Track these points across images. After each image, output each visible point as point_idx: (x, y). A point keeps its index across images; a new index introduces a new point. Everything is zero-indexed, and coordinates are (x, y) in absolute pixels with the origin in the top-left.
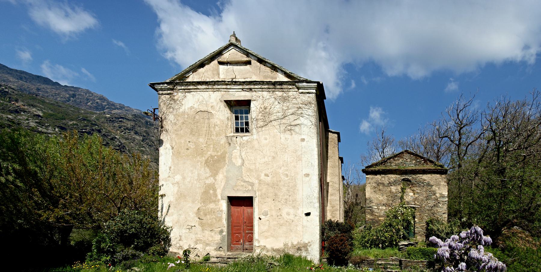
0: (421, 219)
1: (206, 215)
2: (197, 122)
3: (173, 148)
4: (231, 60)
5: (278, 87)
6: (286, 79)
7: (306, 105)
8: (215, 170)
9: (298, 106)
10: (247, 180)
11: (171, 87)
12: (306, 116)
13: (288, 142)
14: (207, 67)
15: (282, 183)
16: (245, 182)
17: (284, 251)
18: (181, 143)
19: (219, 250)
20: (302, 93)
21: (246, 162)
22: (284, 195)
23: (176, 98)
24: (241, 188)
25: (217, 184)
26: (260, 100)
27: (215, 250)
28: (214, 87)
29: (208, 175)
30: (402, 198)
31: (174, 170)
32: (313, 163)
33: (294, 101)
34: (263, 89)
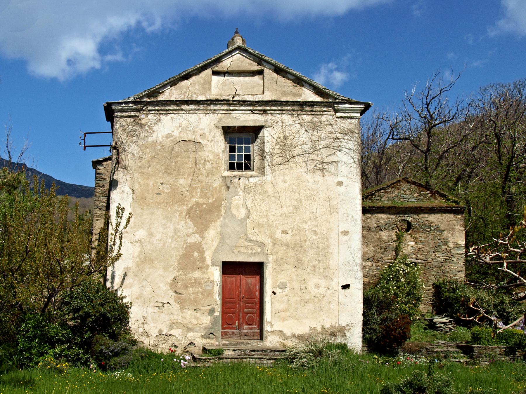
0: (427, 279)
1: (187, 287)
2: (177, 156)
3: (133, 192)
4: (234, 69)
5: (307, 109)
6: (318, 99)
7: (346, 134)
8: (202, 224)
9: (334, 136)
10: (254, 239)
11: (138, 107)
12: (345, 150)
13: (319, 186)
14: (194, 79)
15: (308, 243)
16: (250, 241)
17: (310, 336)
18: (148, 185)
19: (209, 338)
20: (341, 117)
21: (253, 214)
22: (311, 261)
23: (143, 122)
24: (245, 251)
25: (206, 244)
26: (277, 128)
27: (203, 337)
28: (209, 108)
29: (191, 231)
30: (397, 249)
31: (134, 222)
32: (355, 216)
33: (329, 128)
34: (284, 110)
